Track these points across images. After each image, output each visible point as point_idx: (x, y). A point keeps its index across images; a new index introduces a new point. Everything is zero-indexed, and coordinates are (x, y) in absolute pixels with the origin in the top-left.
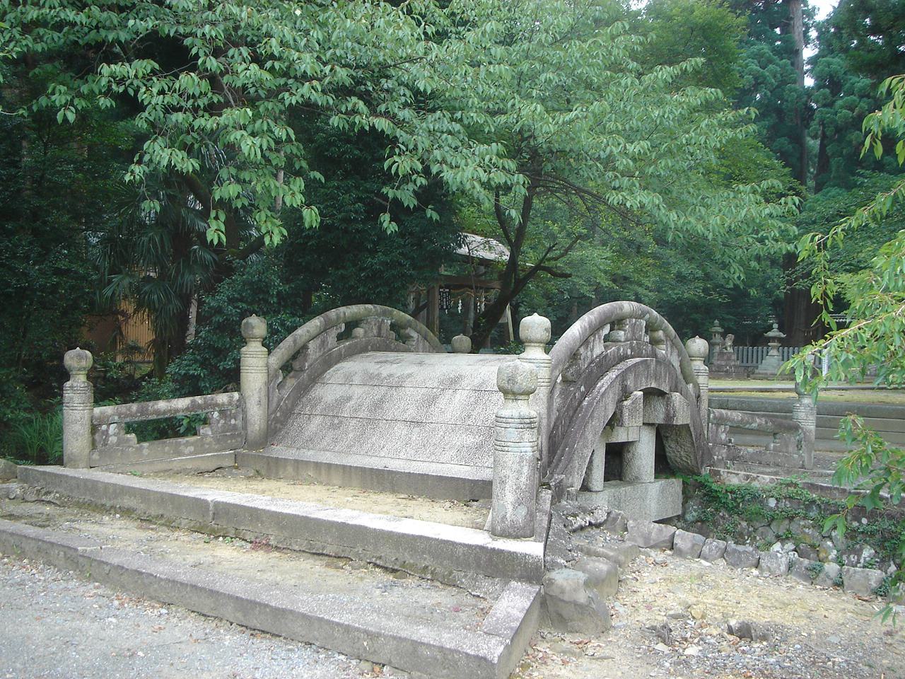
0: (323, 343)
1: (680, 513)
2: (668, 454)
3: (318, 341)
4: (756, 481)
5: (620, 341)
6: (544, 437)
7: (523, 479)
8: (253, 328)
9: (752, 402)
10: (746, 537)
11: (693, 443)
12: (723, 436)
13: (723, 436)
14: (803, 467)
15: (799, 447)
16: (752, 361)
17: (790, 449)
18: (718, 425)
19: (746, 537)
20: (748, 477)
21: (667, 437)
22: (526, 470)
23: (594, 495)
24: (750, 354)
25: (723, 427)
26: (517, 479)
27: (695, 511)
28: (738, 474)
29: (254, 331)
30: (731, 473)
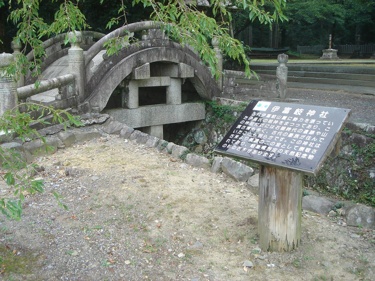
0: (53, 49)
1: (204, 118)
2: (198, 92)
3: (51, 48)
4: (233, 104)
5: (145, 40)
6: (79, 85)
7: (6, 104)
8: (13, 45)
9: (318, 68)
10: (225, 130)
11: (204, 86)
12: (232, 83)
13: (232, 83)
14: (279, 97)
15: (277, 87)
16: (345, 51)
17: (272, 89)
18: (229, 78)
19: (225, 130)
20: (230, 102)
21: (194, 84)
22: (7, 100)
23: (129, 111)
24: (350, 49)
25: (232, 79)
26: (4, 104)
27: (209, 118)
28: (226, 100)
29: (14, 46)
30: (224, 100)
